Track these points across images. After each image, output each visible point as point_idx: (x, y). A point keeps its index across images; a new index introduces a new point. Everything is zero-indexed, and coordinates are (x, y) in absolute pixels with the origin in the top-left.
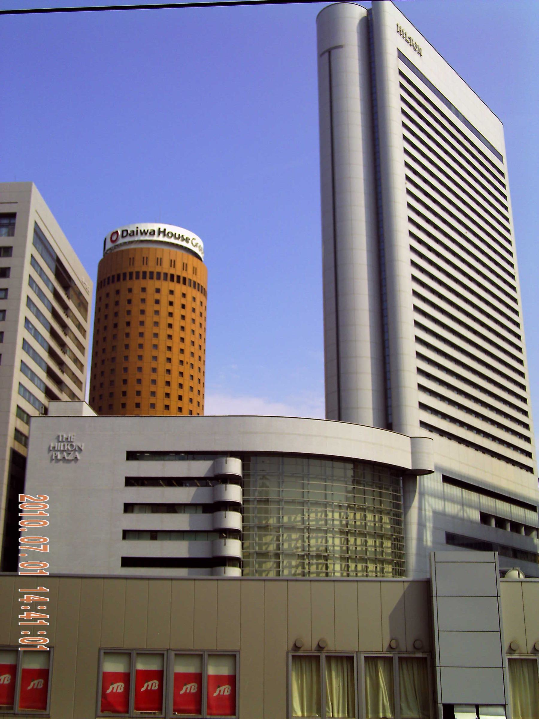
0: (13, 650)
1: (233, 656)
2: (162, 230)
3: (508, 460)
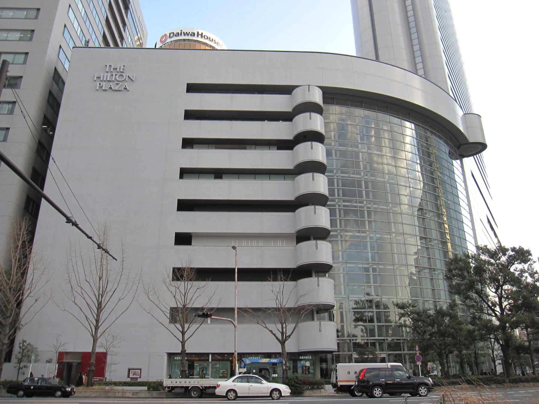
0: (533, 324)
1: (140, 370)
2: (200, 33)
3: (348, 381)
